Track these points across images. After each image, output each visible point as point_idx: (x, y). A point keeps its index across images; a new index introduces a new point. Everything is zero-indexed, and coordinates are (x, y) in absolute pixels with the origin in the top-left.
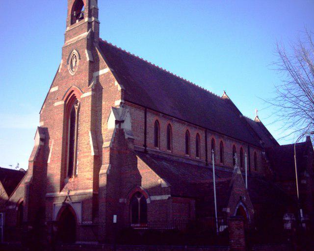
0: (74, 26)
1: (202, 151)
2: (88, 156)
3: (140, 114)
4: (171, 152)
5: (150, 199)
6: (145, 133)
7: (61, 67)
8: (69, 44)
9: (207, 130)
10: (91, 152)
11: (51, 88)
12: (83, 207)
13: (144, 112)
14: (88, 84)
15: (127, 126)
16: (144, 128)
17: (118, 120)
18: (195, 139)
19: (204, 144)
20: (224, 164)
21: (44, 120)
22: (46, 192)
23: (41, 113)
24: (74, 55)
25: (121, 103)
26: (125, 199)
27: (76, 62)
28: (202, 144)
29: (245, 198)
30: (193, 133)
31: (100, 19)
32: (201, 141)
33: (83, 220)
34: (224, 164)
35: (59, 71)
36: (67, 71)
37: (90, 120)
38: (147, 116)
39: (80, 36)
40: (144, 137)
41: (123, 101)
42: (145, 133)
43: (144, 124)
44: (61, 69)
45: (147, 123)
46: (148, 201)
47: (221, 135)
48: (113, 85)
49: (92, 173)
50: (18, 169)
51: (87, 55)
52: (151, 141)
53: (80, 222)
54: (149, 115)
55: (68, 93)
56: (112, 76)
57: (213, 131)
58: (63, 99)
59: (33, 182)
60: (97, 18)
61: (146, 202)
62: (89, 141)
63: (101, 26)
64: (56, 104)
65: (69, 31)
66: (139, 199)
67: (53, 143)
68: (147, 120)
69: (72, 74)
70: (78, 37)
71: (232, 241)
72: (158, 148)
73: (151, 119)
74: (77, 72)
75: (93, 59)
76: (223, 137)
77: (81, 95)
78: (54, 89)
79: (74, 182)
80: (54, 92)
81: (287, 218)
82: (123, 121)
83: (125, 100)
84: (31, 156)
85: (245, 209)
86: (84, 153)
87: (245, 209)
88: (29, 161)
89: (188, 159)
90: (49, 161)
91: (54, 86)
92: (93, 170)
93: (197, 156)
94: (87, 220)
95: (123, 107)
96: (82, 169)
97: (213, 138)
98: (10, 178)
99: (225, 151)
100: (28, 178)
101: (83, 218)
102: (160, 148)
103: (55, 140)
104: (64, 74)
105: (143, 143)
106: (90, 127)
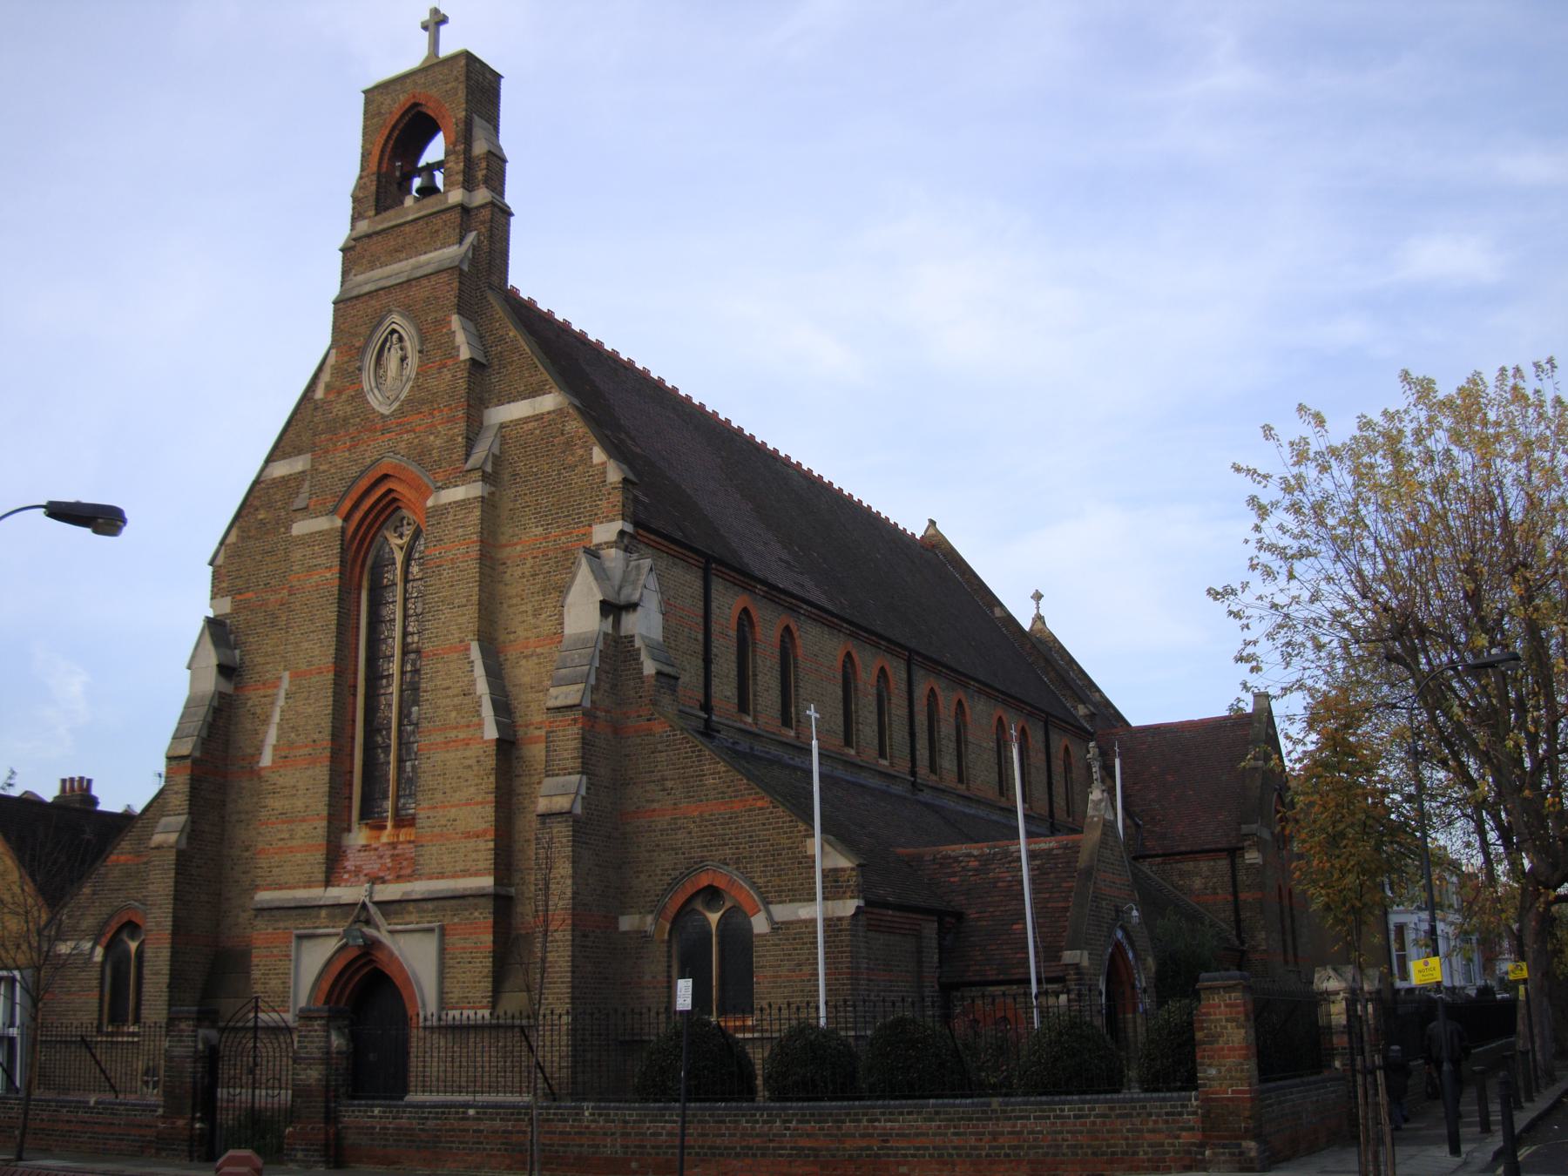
0: (391, 218)
1: (898, 733)
2: (466, 743)
3: (689, 581)
4: (792, 733)
5: (769, 912)
6: (707, 661)
7: (326, 377)
8: (367, 288)
9: (913, 658)
10: (480, 725)
11: (269, 460)
12: (442, 950)
13: (700, 573)
14: (461, 452)
15: (645, 625)
16: (701, 637)
17: (611, 598)
18: (874, 691)
19: (904, 712)
20: (968, 789)
21: (234, 592)
22: (257, 888)
23: (220, 561)
24: (394, 331)
25: (622, 533)
26: (649, 919)
27: (403, 359)
28: (898, 709)
29: (1135, 913)
30: (868, 664)
31: (513, 196)
32: (894, 700)
33: (443, 1004)
34: (968, 789)
35: (319, 394)
36: (360, 396)
37: (475, 598)
38: (714, 594)
39: (423, 258)
40: (701, 672)
41: (629, 528)
42: (707, 661)
43: (700, 620)
44: (328, 387)
45: (714, 617)
46: (760, 924)
47: (959, 678)
48: (586, 460)
49: (489, 811)
50: (15, 792)
51: (460, 338)
52: (725, 690)
53: (432, 1007)
54: (717, 586)
55: (364, 483)
56: (576, 426)
57: (935, 665)
58: (333, 512)
59: (189, 843)
60: (502, 194)
61: (750, 929)
62: (473, 683)
63: (516, 228)
64: (300, 528)
65: (369, 236)
66: (714, 918)
67: (285, 684)
68: (714, 605)
69: (385, 411)
70: (412, 261)
71: (1213, 1072)
72: (749, 720)
73: (728, 604)
74: (408, 401)
75: (486, 354)
76: (965, 686)
77: (426, 499)
78: (281, 469)
79: (393, 845)
80: (285, 480)
81: (1333, 984)
82: (632, 607)
83: (636, 524)
84: (177, 737)
85: (1130, 955)
86: (444, 728)
87: (1130, 955)
88: (170, 758)
89: (854, 765)
90: (266, 760)
91: (286, 455)
92: (491, 797)
93: (882, 754)
94: (465, 1003)
95: (626, 550)
96: (439, 796)
97: (932, 690)
98: (60, 836)
99: (970, 738)
100: (168, 833)
101: (442, 993)
102: (755, 718)
103: (296, 675)
104: (340, 408)
105: (700, 695)
106: (474, 626)
